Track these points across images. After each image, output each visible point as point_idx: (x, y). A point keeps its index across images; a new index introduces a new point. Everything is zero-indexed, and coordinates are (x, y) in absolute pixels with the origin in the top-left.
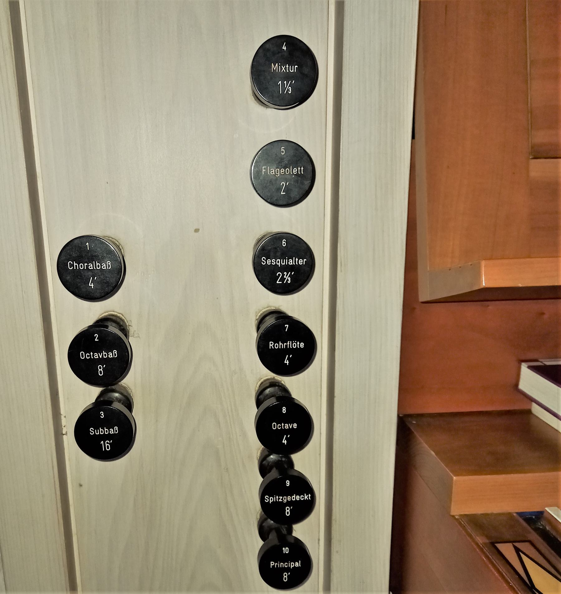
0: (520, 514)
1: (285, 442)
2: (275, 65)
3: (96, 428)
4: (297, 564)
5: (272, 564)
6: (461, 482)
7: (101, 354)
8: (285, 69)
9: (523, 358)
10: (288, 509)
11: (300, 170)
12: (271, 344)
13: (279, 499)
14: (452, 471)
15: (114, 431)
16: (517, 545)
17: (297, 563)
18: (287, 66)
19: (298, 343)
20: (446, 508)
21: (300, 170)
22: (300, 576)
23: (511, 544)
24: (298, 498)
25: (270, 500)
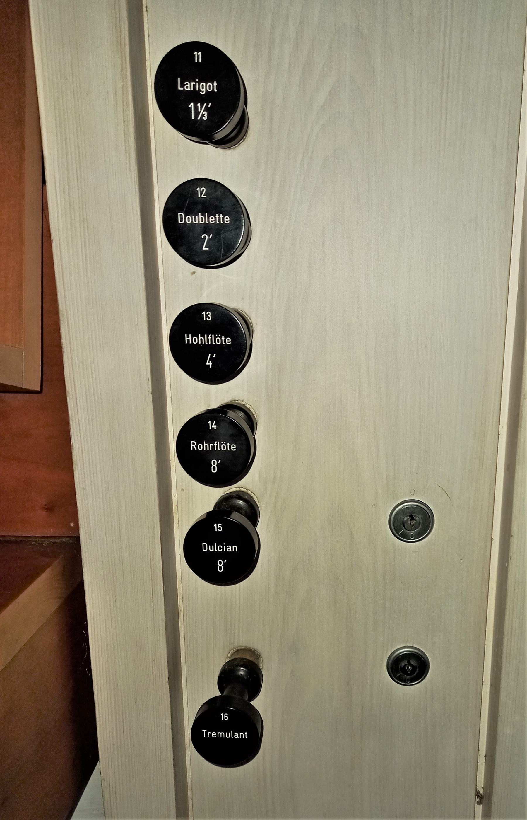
10: (220, 563)
19: (223, 338)
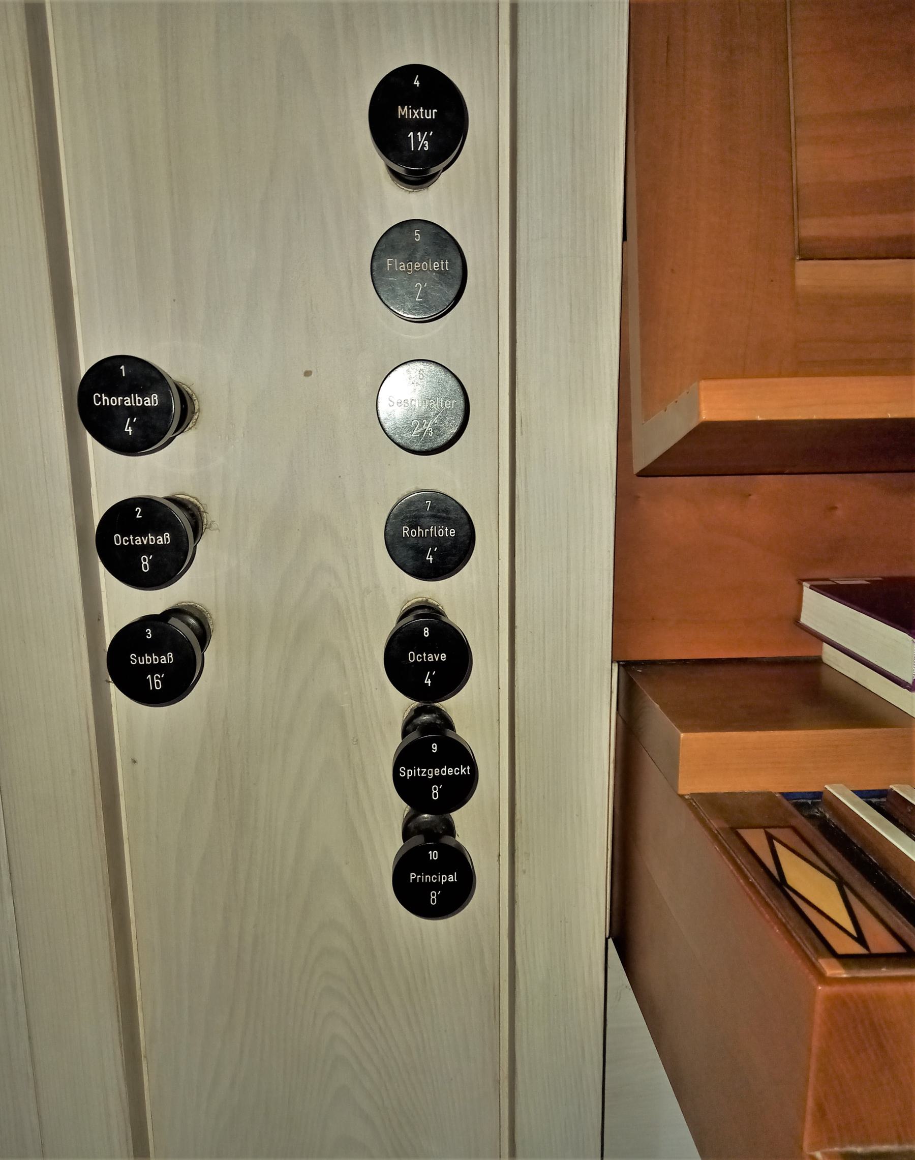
0: (787, 796)
1: (428, 682)
2: (403, 109)
3: (141, 654)
4: (452, 878)
5: (412, 876)
6: (693, 742)
7: (144, 540)
8: (419, 114)
9: (806, 577)
11: (444, 265)
12: (406, 529)
13: (421, 772)
14: (680, 727)
15: (167, 659)
16: (772, 831)
17: (451, 877)
18: (422, 110)
20: (673, 785)
21: (444, 265)
22: (455, 898)
23: (762, 830)
24: (450, 771)
25: (407, 773)
